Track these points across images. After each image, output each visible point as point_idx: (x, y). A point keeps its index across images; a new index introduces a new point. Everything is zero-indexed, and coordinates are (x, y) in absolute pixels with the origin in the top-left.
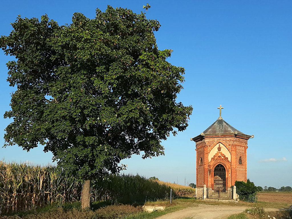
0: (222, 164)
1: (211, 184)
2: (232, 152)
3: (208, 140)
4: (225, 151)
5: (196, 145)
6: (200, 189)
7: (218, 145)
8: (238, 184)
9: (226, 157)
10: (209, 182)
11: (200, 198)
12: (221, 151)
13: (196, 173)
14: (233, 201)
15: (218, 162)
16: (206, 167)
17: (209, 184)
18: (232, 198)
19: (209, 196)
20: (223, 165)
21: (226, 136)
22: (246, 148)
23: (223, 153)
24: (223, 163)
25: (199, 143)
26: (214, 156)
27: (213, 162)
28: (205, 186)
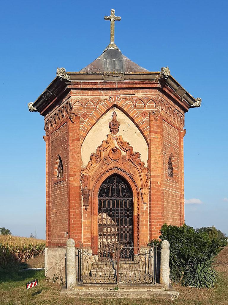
0: (123, 174)
1: (89, 235)
2: (153, 136)
3: (79, 98)
4: (129, 133)
5: (46, 124)
6: (56, 251)
7: (110, 114)
8: (171, 233)
9: (135, 151)
10: (85, 229)
11: (57, 278)
12: (118, 134)
13: (44, 206)
14: (161, 290)
15: (110, 166)
16: (75, 182)
17: (85, 236)
18: (158, 281)
19: (83, 274)
20: (127, 177)
21: (136, 86)
22: (182, 133)
23: (125, 139)
24: (129, 170)
25: (53, 114)
26: (100, 149)
27: (96, 167)
28: (71, 242)
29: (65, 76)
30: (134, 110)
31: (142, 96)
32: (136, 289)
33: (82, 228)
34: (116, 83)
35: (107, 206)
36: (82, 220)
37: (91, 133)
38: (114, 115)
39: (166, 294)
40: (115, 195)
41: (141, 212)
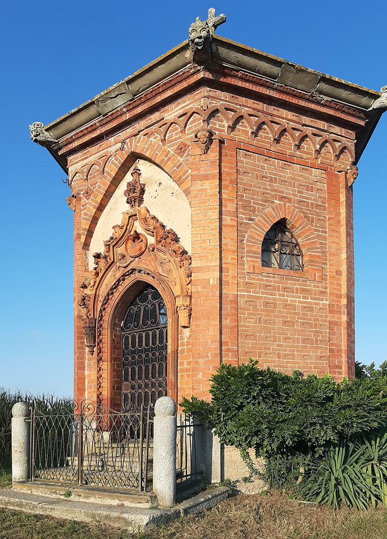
29: (41, 135)
30: (163, 148)
31: (176, 114)
32: (100, 498)
33: (86, 386)
34: (125, 110)
35: (137, 344)
36: (86, 373)
37: (102, 220)
38: (137, 172)
39: (119, 518)
40: (149, 322)
41: (181, 347)
